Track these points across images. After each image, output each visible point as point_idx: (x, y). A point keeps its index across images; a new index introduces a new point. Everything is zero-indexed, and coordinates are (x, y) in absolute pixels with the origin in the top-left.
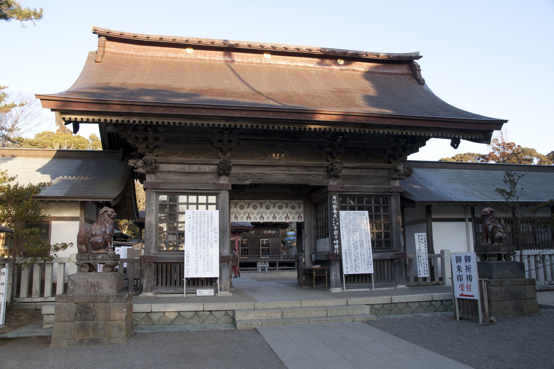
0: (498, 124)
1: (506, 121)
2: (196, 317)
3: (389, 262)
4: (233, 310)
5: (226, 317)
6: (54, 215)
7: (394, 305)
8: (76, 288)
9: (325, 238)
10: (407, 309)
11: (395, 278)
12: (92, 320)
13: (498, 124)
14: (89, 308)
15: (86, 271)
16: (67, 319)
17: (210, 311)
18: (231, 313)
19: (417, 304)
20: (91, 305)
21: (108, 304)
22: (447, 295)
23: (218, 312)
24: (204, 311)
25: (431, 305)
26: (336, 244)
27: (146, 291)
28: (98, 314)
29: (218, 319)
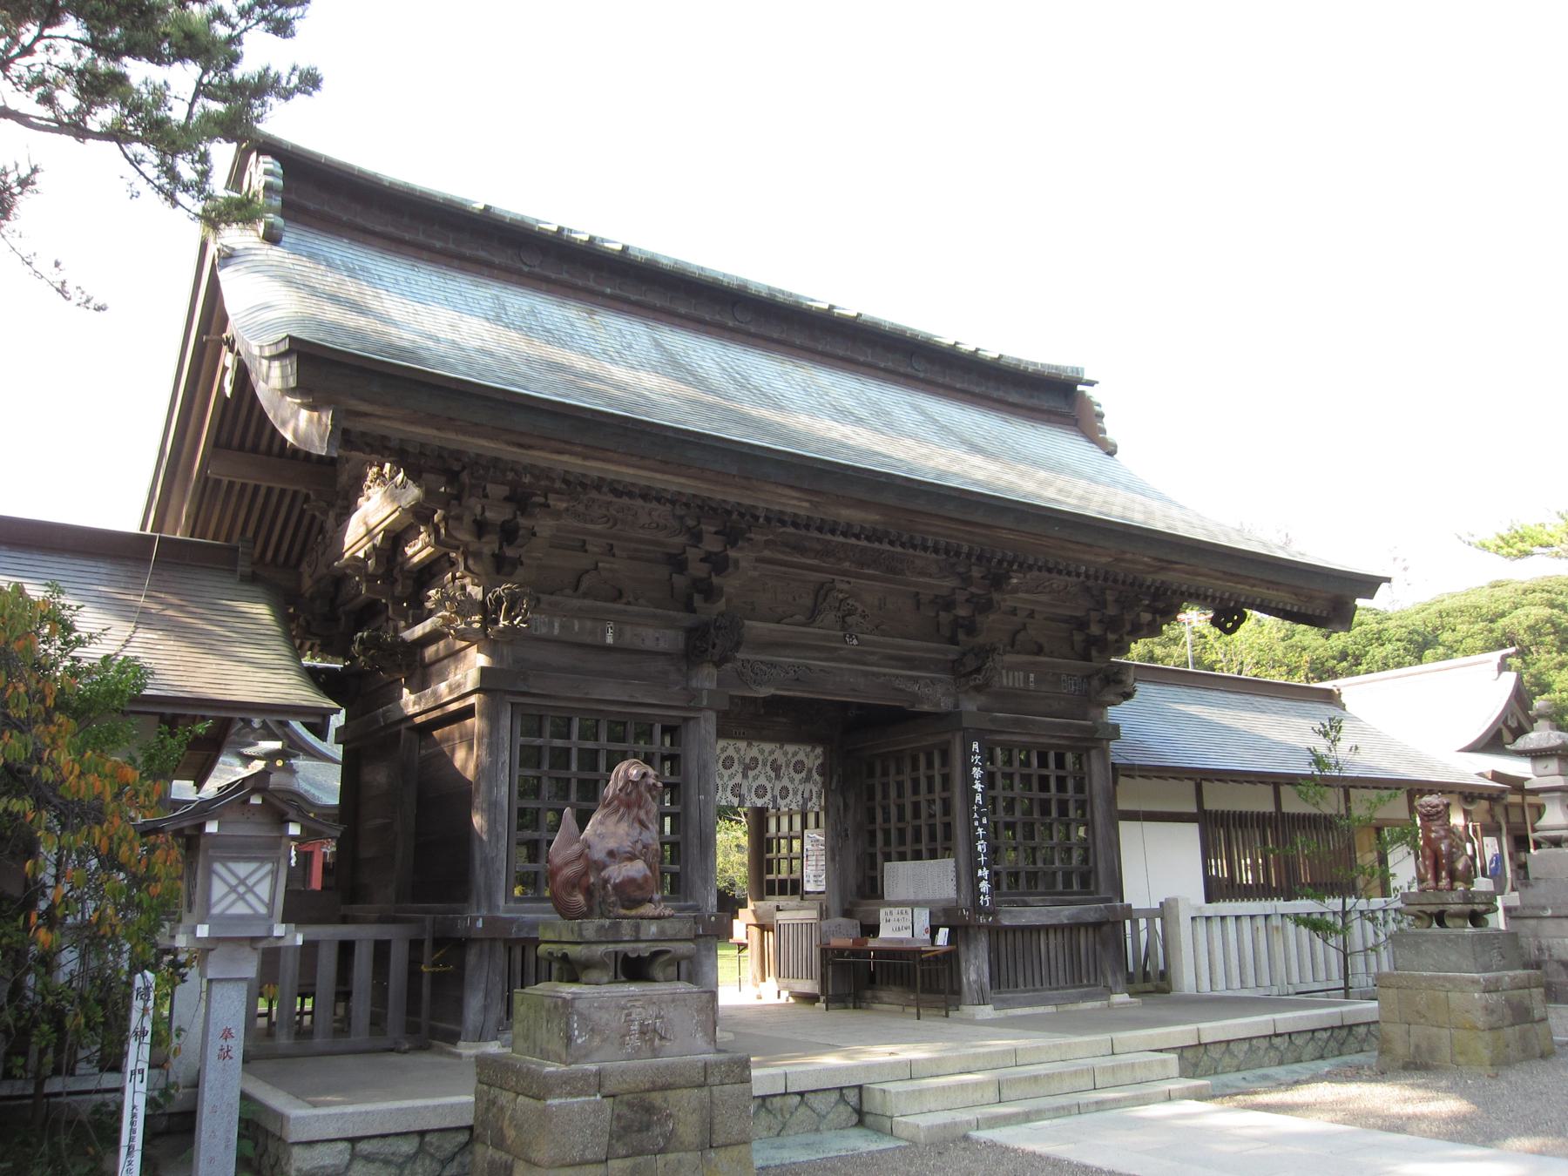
0: (1369, 585)
1: (1388, 580)
2: (763, 1113)
3: (1090, 931)
4: (860, 1087)
5: (841, 1107)
6: (1504, 840)
7: (1202, 1049)
8: (597, 1041)
9: (933, 855)
10: (1227, 1059)
11: (1105, 977)
12: (662, 1151)
13: (1369, 585)
14: (650, 1109)
15: (606, 979)
16: (589, 1155)
17: (801, 1094)
18: (852, 1097)
19: (1246, 1046)
20: (657, 1098)
21: (705, 1092)
22: (1301, 1018)
23: (820, 1095)
24: (786, 1094)
25: (1272, 1045)
26: (982, 878)
27: (481, 1037)
28: (681, 1129)
29: (822, 1117)
